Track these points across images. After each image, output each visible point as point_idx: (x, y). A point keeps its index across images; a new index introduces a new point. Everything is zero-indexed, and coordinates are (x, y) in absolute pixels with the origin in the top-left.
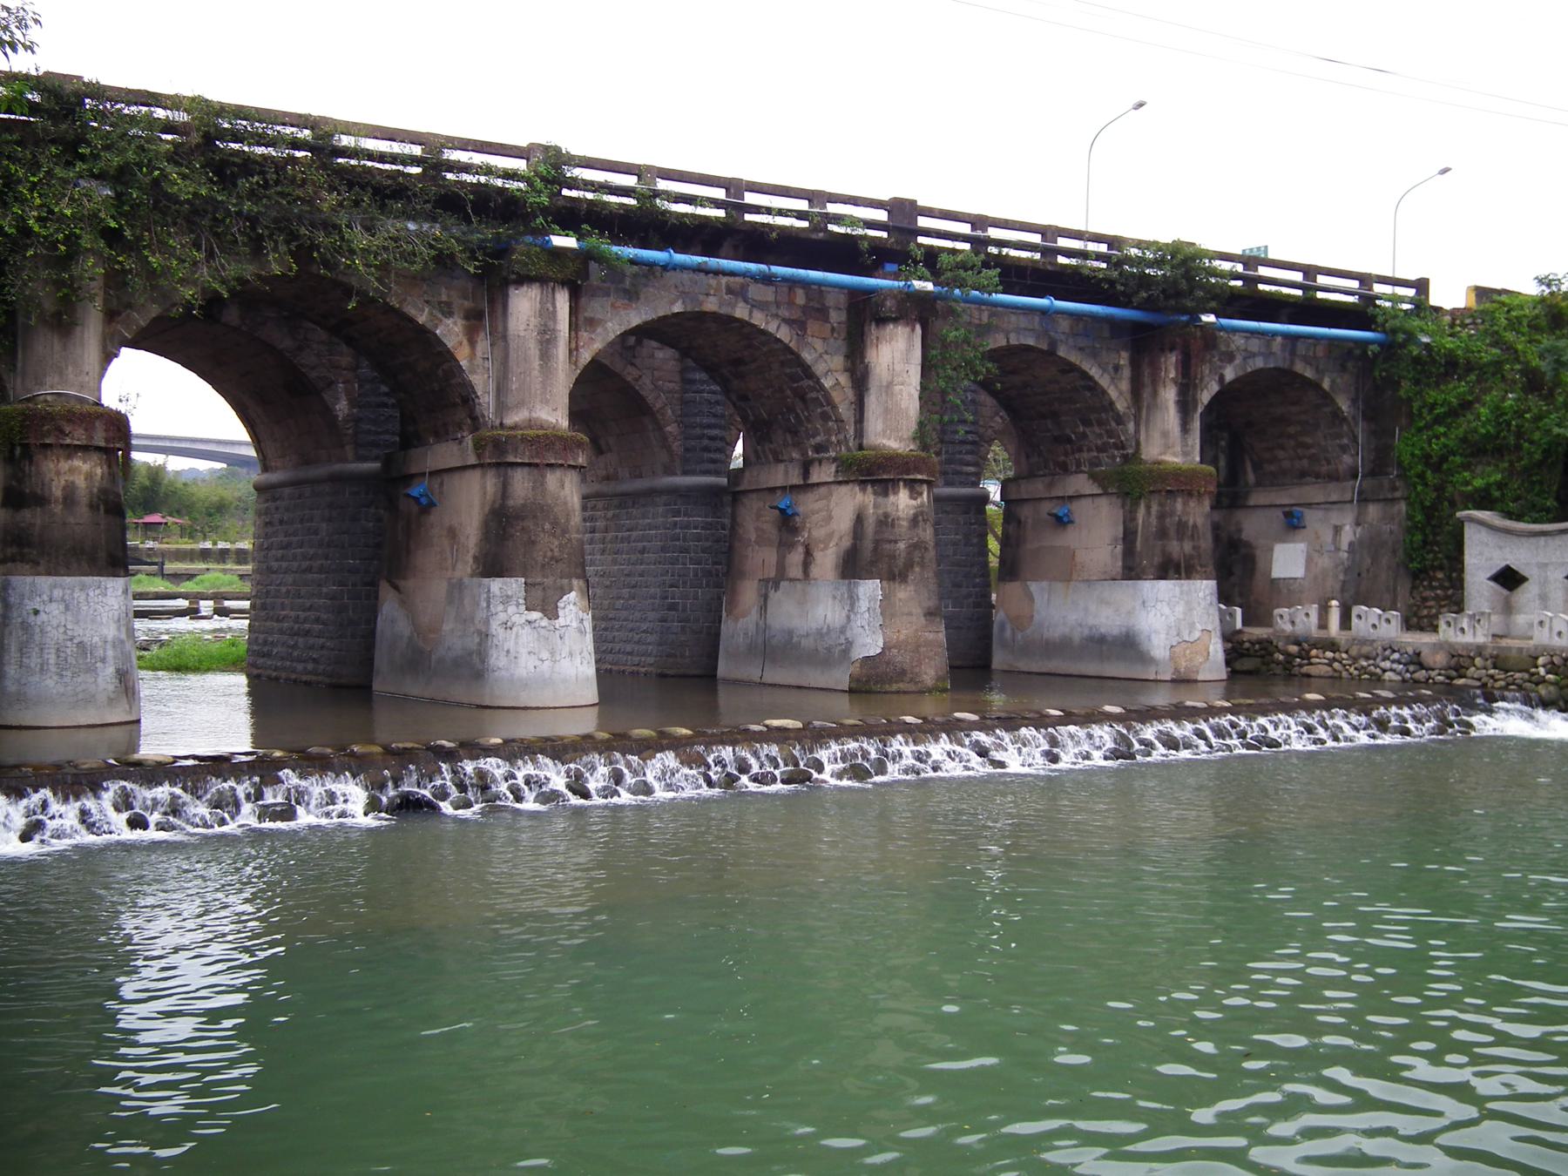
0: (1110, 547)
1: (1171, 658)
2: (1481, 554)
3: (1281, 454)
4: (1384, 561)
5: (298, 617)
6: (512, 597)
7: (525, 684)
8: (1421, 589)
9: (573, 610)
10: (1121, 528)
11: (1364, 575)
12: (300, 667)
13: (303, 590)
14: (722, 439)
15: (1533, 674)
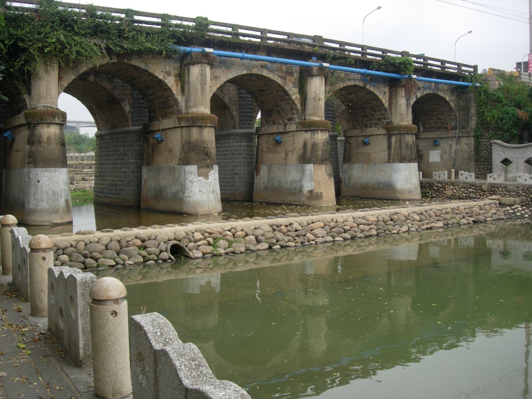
3: (431, 121)
5: (112, 179)
9: (214, 175)
12: (114, 196)
13: (114, 170)
14: (252, 116)
15: (518, 193)
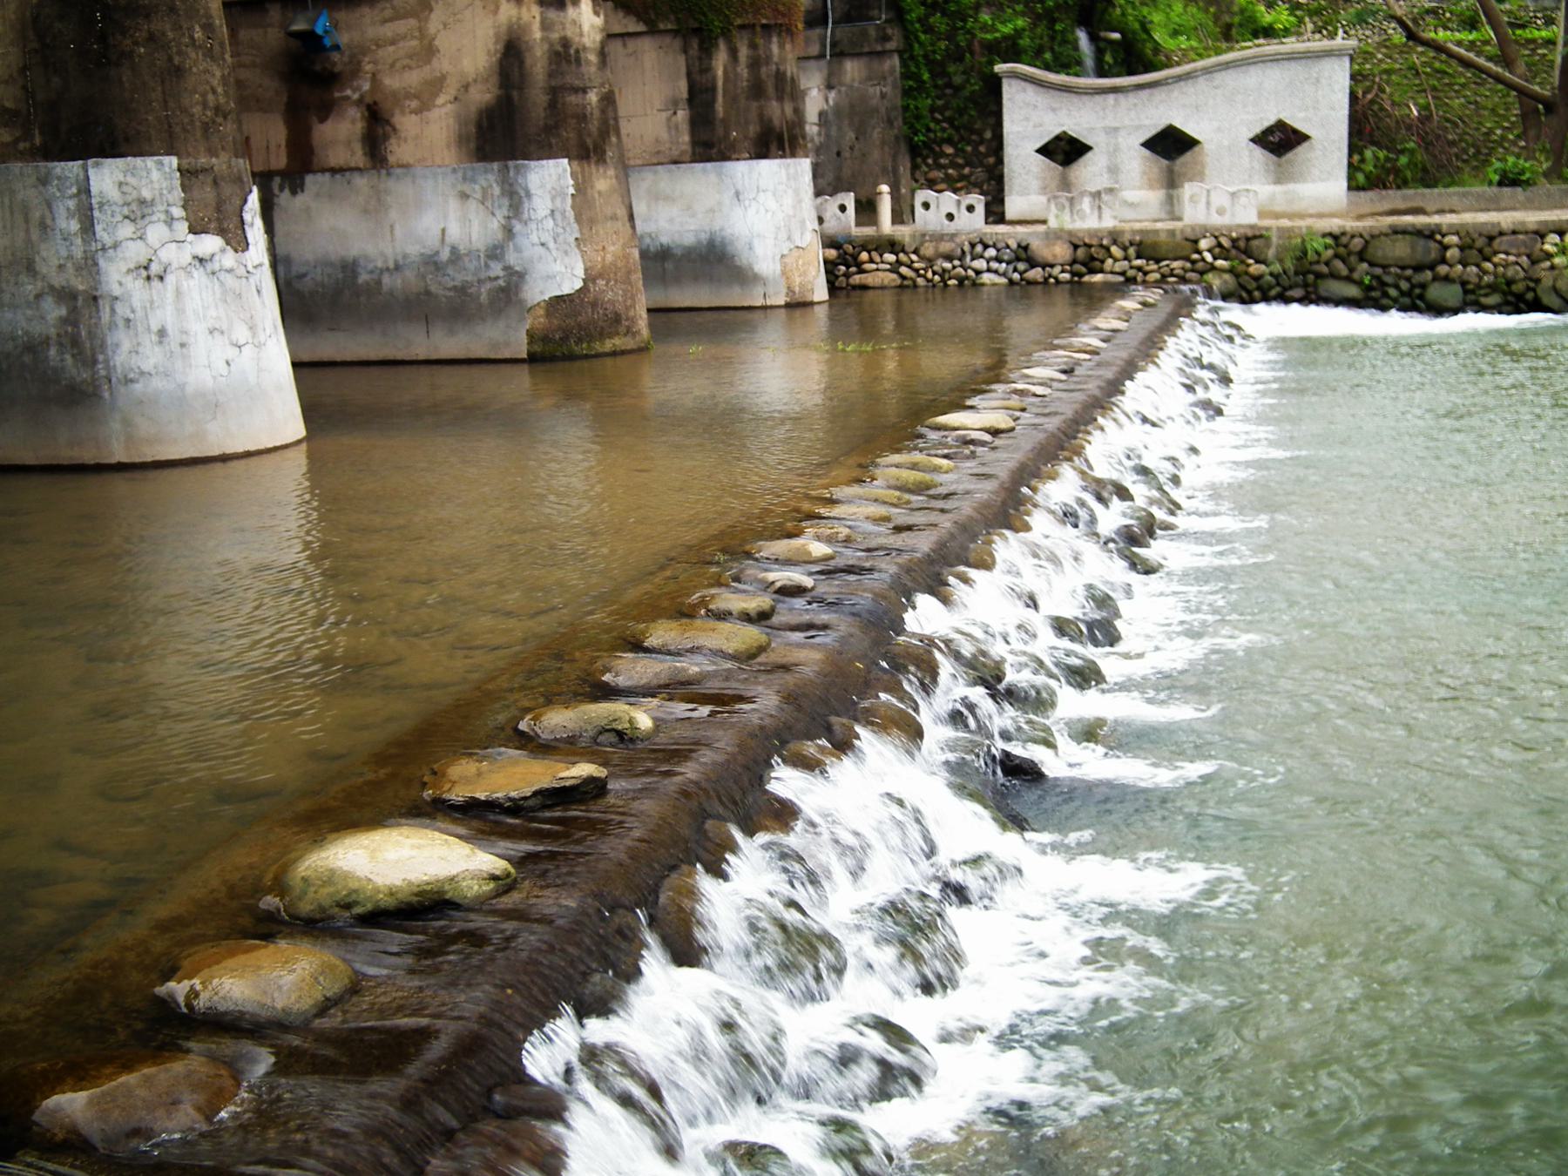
0: (665, 115)
1: (784, 273)
2: (1027, 119)
4: (876, 134)
6: (152, 203)
7: (214, 404)
8: (925, 168)
10: (683, 85)
11: (846, 154)
